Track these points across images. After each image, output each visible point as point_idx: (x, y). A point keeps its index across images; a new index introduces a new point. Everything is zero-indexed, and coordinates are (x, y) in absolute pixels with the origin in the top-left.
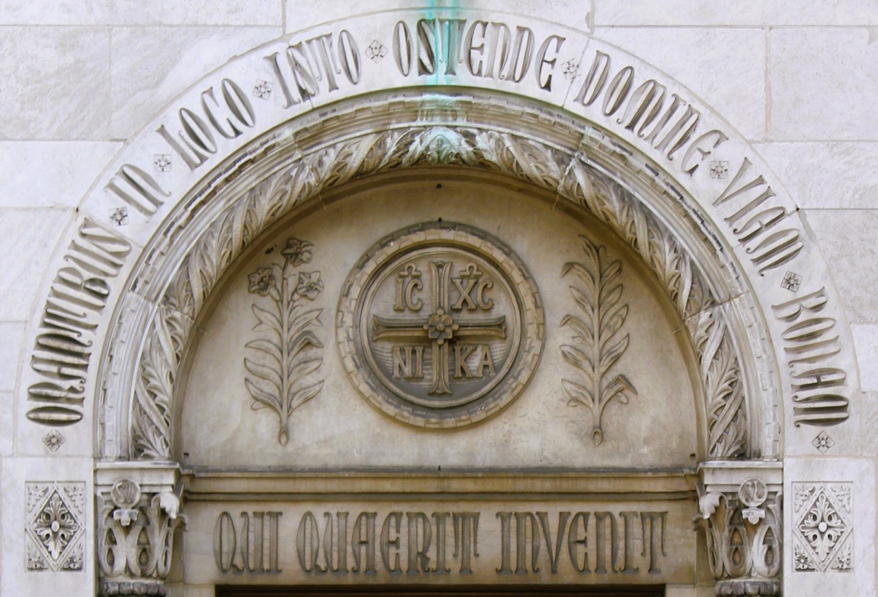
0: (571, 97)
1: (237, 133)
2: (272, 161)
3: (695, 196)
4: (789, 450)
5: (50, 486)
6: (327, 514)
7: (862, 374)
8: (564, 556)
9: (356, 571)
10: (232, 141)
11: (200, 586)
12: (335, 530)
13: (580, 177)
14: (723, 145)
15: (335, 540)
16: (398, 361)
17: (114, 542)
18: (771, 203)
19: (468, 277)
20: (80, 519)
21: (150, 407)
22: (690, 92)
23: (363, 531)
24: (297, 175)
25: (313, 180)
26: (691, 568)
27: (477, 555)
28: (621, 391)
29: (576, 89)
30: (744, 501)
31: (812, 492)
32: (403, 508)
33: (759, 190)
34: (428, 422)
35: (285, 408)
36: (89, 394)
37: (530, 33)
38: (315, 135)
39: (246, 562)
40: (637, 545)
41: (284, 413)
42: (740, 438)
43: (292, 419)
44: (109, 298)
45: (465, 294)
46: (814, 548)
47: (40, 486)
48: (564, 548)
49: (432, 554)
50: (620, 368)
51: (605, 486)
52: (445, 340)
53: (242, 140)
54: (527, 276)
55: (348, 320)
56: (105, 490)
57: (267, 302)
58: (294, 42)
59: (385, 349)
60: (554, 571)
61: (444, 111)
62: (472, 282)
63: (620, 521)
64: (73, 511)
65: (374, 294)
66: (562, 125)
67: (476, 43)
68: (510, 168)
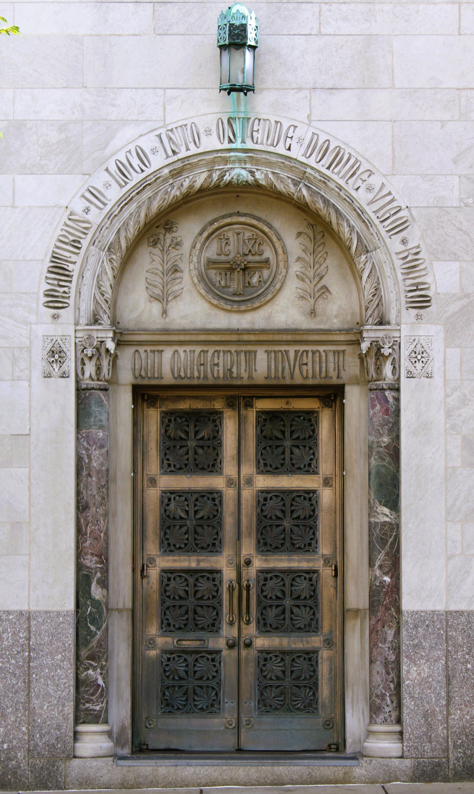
0: (300, 154)
1: (143, 171)
4: (403, 321)
5: (54, 338)
8: (297, 371)
9: (198, 378)
11: (125, 385)
12: (189, 359)
14: (372, 177)
15: (189, 363)
16: (218, 279)
18: (395, 204)
19: (252, 239)
20: (68, 353)
21: (101, 300)
22: (356, 152)
23: (202, 359)
24: (171, 191)
25: (178, 193)
26: (357, 376)
27: (256, 370)
28: (324, 293)
30: (382, 345)
31: (414, 340)
32: (221, 348)
33: (389, 198)
35: (165, 301)
36: (72, 294)
37: (281, 124)
39: (146, 373)
40: (331, 365)
42: (380, 315)
43: (168, 306)
44: (82, 249)
45: (250, 247)
46: (415, 367)
47: (49, 338)
48: (297, 367)
49: (234, 370)
50: (323, 282)
51: (316, 338)
52: (241, 269)
53: (145, 175)
54: (279, 239)
55: (195, 259)
56: (80, 339)
57: (156, 251)
58: (169, 128)
59: (212, 273)
60: (292, 378)
61: (240, 161)
62: (253, 241)
63: (323, 354)
64: (65, 350)
66: (296, 167)
67: (255, 129)
68: (272, 188)
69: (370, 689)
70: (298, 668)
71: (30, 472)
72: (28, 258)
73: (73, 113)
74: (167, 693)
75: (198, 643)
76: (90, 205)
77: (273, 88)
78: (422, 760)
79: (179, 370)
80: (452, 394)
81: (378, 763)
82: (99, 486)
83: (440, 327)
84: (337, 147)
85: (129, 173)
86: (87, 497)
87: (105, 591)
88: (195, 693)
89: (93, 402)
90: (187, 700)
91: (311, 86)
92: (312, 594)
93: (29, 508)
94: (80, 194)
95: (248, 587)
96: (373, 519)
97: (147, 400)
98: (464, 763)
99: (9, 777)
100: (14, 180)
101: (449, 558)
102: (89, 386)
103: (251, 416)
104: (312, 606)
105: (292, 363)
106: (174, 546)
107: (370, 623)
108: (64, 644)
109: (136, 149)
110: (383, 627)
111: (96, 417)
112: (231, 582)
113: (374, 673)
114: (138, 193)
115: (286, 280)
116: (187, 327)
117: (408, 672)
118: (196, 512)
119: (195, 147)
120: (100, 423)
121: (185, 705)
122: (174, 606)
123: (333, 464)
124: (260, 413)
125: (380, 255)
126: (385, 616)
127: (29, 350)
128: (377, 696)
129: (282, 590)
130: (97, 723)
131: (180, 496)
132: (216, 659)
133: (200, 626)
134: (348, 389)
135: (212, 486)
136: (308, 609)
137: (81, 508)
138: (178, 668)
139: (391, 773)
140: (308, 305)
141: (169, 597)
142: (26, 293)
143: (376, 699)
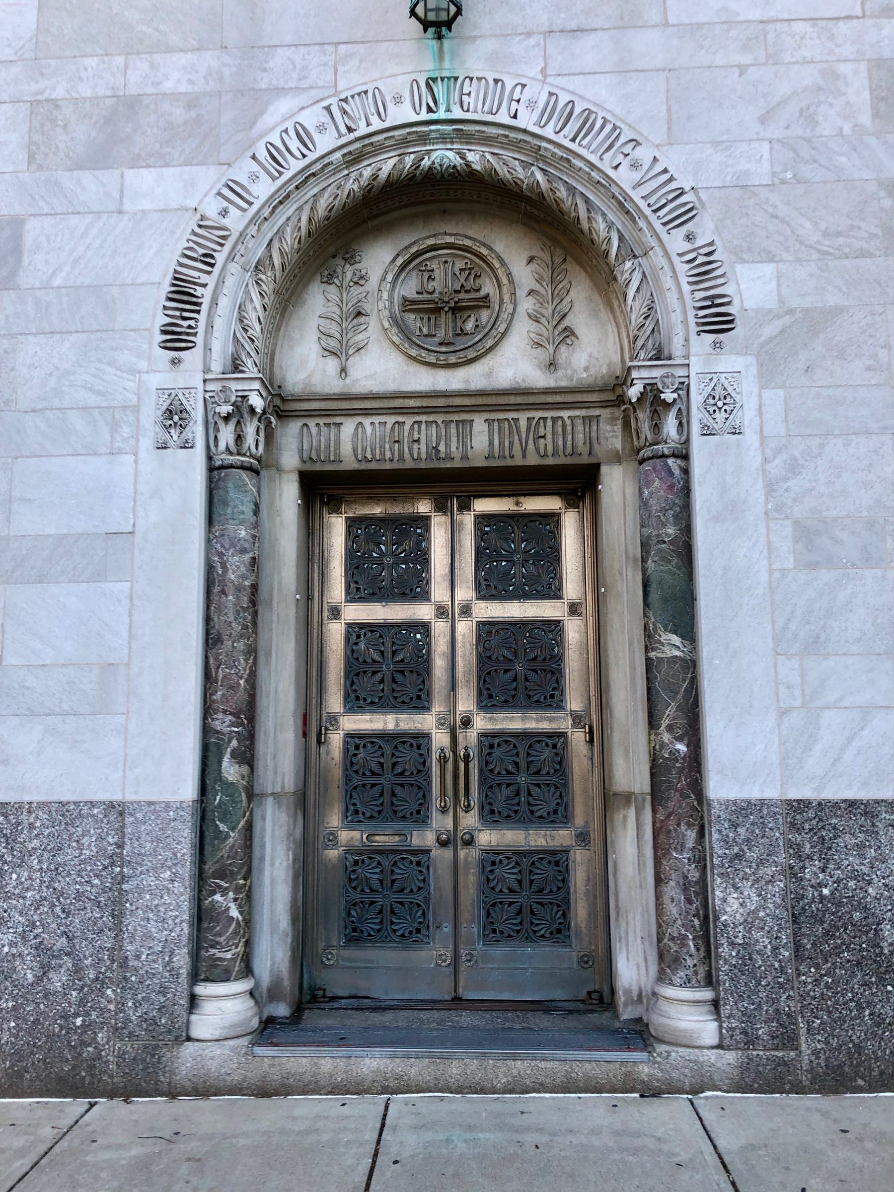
0: (531, 123)
1: (304, 156)
2: (327, 178)
3: (619, 183)
4: (693, 351)
5: (173, 391)
6: (372, 423)
7: (744, 297)
8: (531, 446)
9: (391, 460)
10: (301, 162)
11: (289, 472)
12: (378, 434)
13: (539, 176)
14: (638, 148)
15: (378, 440)
16: (418, 324)
17: (218, 430)
18: (674, 185)
19: (464, 270)
20: (193, 413)
21: (244, 338)
22: (614, 115)
23: (396, 434)
24: (345, 184)
25: (355, 187)
26: (617, 452)
27: (472, 448)
28: (568, 336)
29: (535, 116)
30: (661, 388)
31: (711, 380)
32: (423, 418)
33: (665, 177)
34: (438, 359)
35: (344, 354)
36: (201, 329)
37: (503, 83)
38: (358, 157)
39: (319, 456)
41: (344, 359)
42: (656, 346)
43: (349, 362)
44: (216, 266)
45: (463, 281)
46: (714, 419)
47: (166, 391)
48: (531, 442)
49: (442, 448)
50: (566, 323)
52: (450, 308)
53: (307, 161)
54: (503, 263)
55: (385, 296)
56: (211, 394)
57: (332, 289)
58: (343, 96)
59: (410, 318)
60: (524, 456)
62: (467, 272)
63: (568, 422)
64: (188, 408)
65: (403, 281)
66: (525, 141)
67: (465, 91)
68: (490, 175)
69: (659, 926)
70: (540, 876)
71: (131, 589)
72: (139, 281)
73: (207, 83)
74: (353, 913)
75: (397, 838)
76: (229, 205)
77: (491, 36)
78: (754, 1053)
79: (364, 450)
80: (775, 458)
81: (681, 1057)
82: (238, 608)
83: (750, 359)
84: (585, 110)
85: (286, 160)
86: (219, 625)
87: (245, 769)
88: (393, 912)
89: (230, 485)
90: (381, 922)
91: (545, 28)
92: (558, 767)
93: (129, 643)
94: (215, 191)
95: (467, 757)
96: (654, 653)
97: (327, 504)
98: (827, 1059)
99: (83, 1074)
100: (122, 176)
101: (783, 713)
102: (226, 462)
103: (468, 521)
104: (559, 786)
105: (524, 436)
106: (365, 700)
107: (654, 817)
108: (175, 855)
109: (295, 127)
110: (679, 825)
111: (235, 507)
112: (442, 750)
113: (666, 899)
114: (297, 187)
115: (514, 322)
116: (375, 390)
117: (724, 900)
118: (394, 653)
119: (379, 120)
120: (241, 517)
121: (379, 931)
122: (364, 785)
123: (582, 584)
124: (483, 519)
125: (657, 258)
126: (680, 806)
127: (136, 409)
128: (672, 938)
129: (514, 762)
130: (227, 980)
131: (372, 631)
132: (423, 861)
133: (401, 815)
134: (604, 469)
135: (416, 617)
136: (553, 789)
137: (210, 641)
138: (369, 875)
139: (703, 1075)
140: (543, 355)
141: (356, 772)
142: (134, 330)
143: (671, 944)
